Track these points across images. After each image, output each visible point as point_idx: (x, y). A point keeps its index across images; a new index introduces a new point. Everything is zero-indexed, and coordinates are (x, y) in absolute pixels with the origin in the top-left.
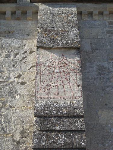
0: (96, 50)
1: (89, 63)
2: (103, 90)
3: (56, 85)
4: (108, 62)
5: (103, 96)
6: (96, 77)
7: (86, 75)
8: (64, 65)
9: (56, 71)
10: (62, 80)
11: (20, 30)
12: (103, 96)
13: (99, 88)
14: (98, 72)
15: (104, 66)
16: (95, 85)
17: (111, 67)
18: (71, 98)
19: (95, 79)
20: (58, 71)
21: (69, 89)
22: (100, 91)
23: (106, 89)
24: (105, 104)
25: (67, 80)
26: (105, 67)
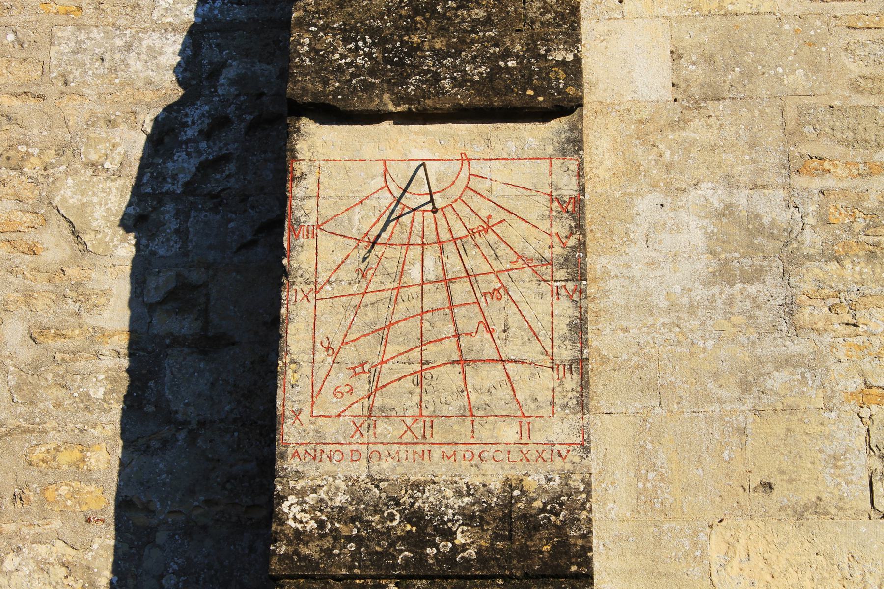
0: (705, 100)
1: (657, 197)
2: (746, 387)
3: (417, 367)
4: (790, 188)
6: (700, 293)
7: (632, 279)
8: (472, 233)
9: (415, 273)
10: (458, 336)
12: (743, 432)
13: (716, 375)
14: (714, 264)
15: (757, 216)
16: (691, 355)
18: (515, 456)
19: (692, 309)
20: (432, 271)
21: (505, 393)
22: (723, 393)
23: (769, 383)
24: (755, 481)
25: (490, 332)
26: (766, 220)
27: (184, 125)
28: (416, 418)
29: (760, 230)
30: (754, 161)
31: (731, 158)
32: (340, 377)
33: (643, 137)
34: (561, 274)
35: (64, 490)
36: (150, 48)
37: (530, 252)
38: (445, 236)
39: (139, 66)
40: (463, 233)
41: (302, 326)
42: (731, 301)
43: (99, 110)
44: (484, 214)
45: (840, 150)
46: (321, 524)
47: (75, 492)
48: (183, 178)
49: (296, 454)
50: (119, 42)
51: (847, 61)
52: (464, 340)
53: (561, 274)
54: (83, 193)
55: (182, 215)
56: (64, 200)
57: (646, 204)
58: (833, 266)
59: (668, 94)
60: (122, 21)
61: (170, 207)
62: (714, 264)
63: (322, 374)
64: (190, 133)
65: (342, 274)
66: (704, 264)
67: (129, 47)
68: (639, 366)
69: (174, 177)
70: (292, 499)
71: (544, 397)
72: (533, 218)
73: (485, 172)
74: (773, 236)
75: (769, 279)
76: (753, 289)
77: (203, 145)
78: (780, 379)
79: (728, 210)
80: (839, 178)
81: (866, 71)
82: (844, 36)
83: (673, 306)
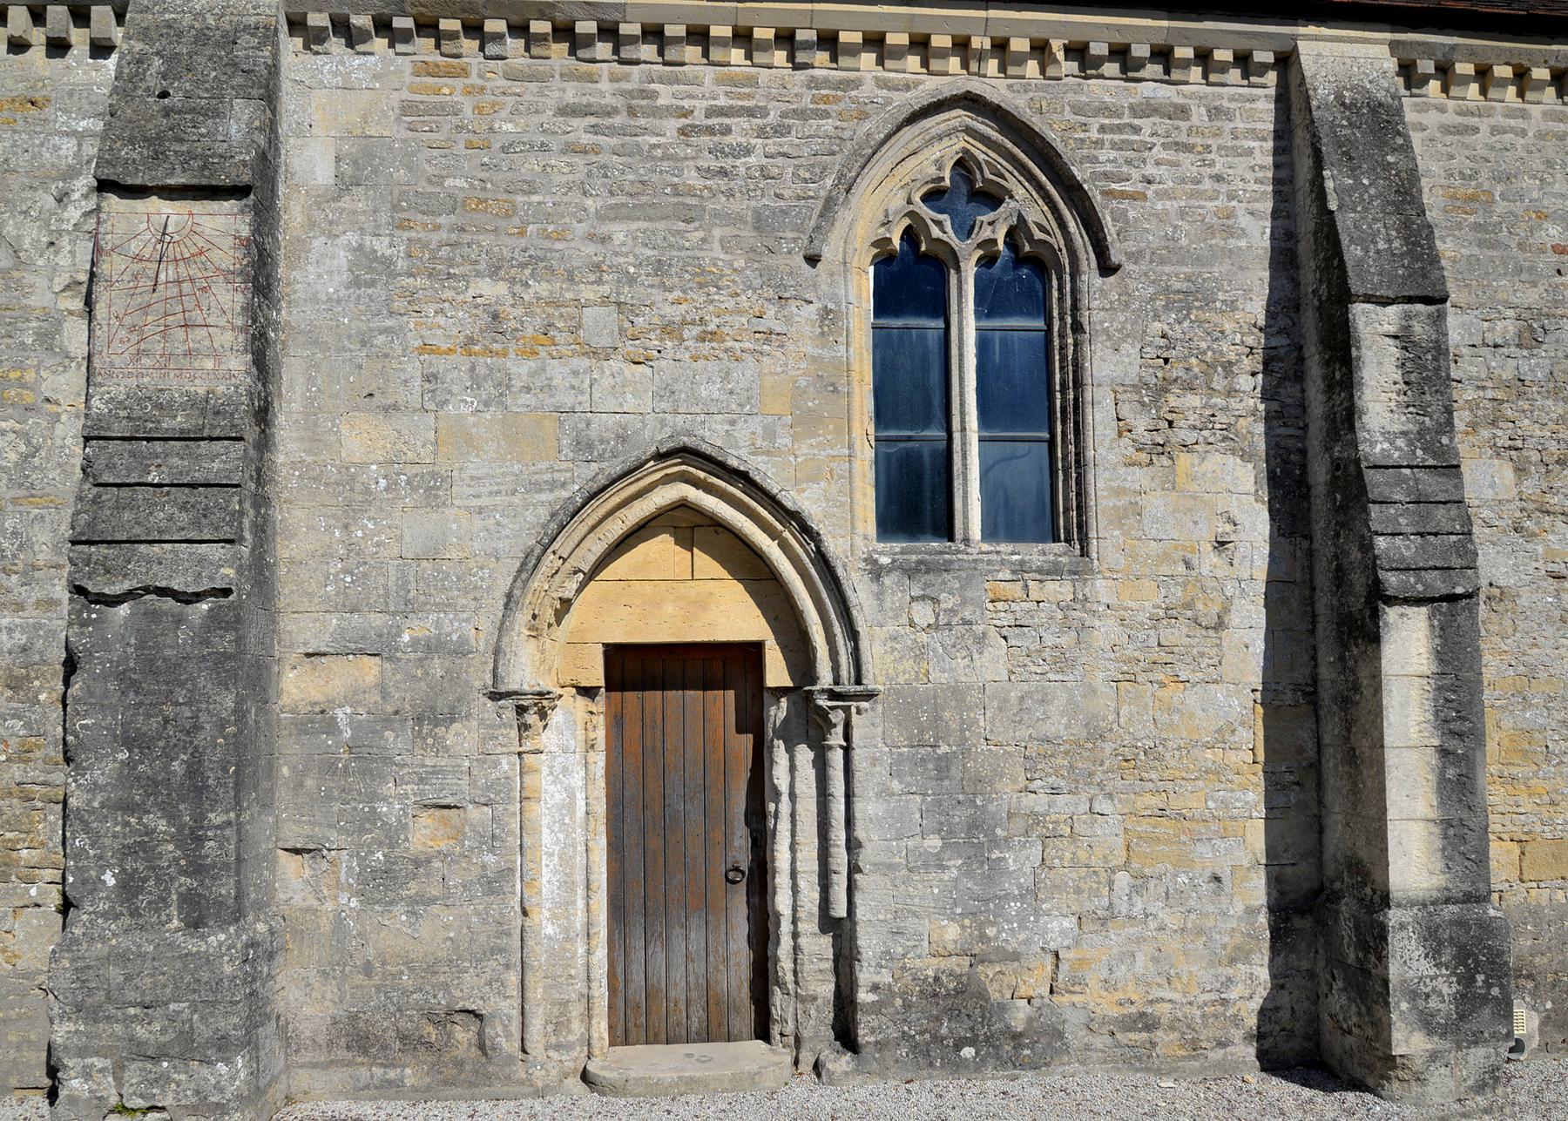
1: (323, 239)
2: (363, 344)
5: (360, 367)
6: (343, 292)
8: (193, 255)
9: (162, 277)
11: (71, 94)
12: (360, 367)
13: (349, 337)
15: (375, 251)
17: (402, 255)
19: (339, 301)
21: (207, 343)
24: (366, 392)
27: (73, 191)
28: (161, 356)
29: (376, 259)
30: (375, 221)
31: (362, 218)
32: (123, 333)
33: (318, 204)
34: (238, 279)
35: (13, 393)
36: (54, 145)
37: (223, 266)
38: (179, 257)
39: (48, 155)
40: (187, 255)
41: (103, 305)
42: (359, 297)
43: (26, 181)
44: (200, 245)
45: (419, 216)
46: (111, 411)
47: (18, 394)
48: (73, 222)
49: (100, 374)
50: (37, 142)
51: (426, 166)
52: (187, 314)
53: (238, 279)
54: (19, 229)
55: (73, 242)
56: (8, 232)
57: (317, 243)
58: (412, 279)
59: (332, 181)
60: (38, 129)
61: (66, 238)
62: (351, 277)
63: (114, 331)
64: (76, 196)
65: (124, 277)
66: (346, 276)
67: (42, 144)
68: (310, 331)
69: (68, 220)
70: (97, 397)
71: (227, 345)
72: (225, 248)
73: (200, 221)
74: (382, 263)
75: (379, 287)
76: (370, 291)
77: (83, 203)
78: (380, 340)
79: (360, 247)
80: (419, 232)
81: (436, 173)
82: (427, 153)
83: (330, 299)
